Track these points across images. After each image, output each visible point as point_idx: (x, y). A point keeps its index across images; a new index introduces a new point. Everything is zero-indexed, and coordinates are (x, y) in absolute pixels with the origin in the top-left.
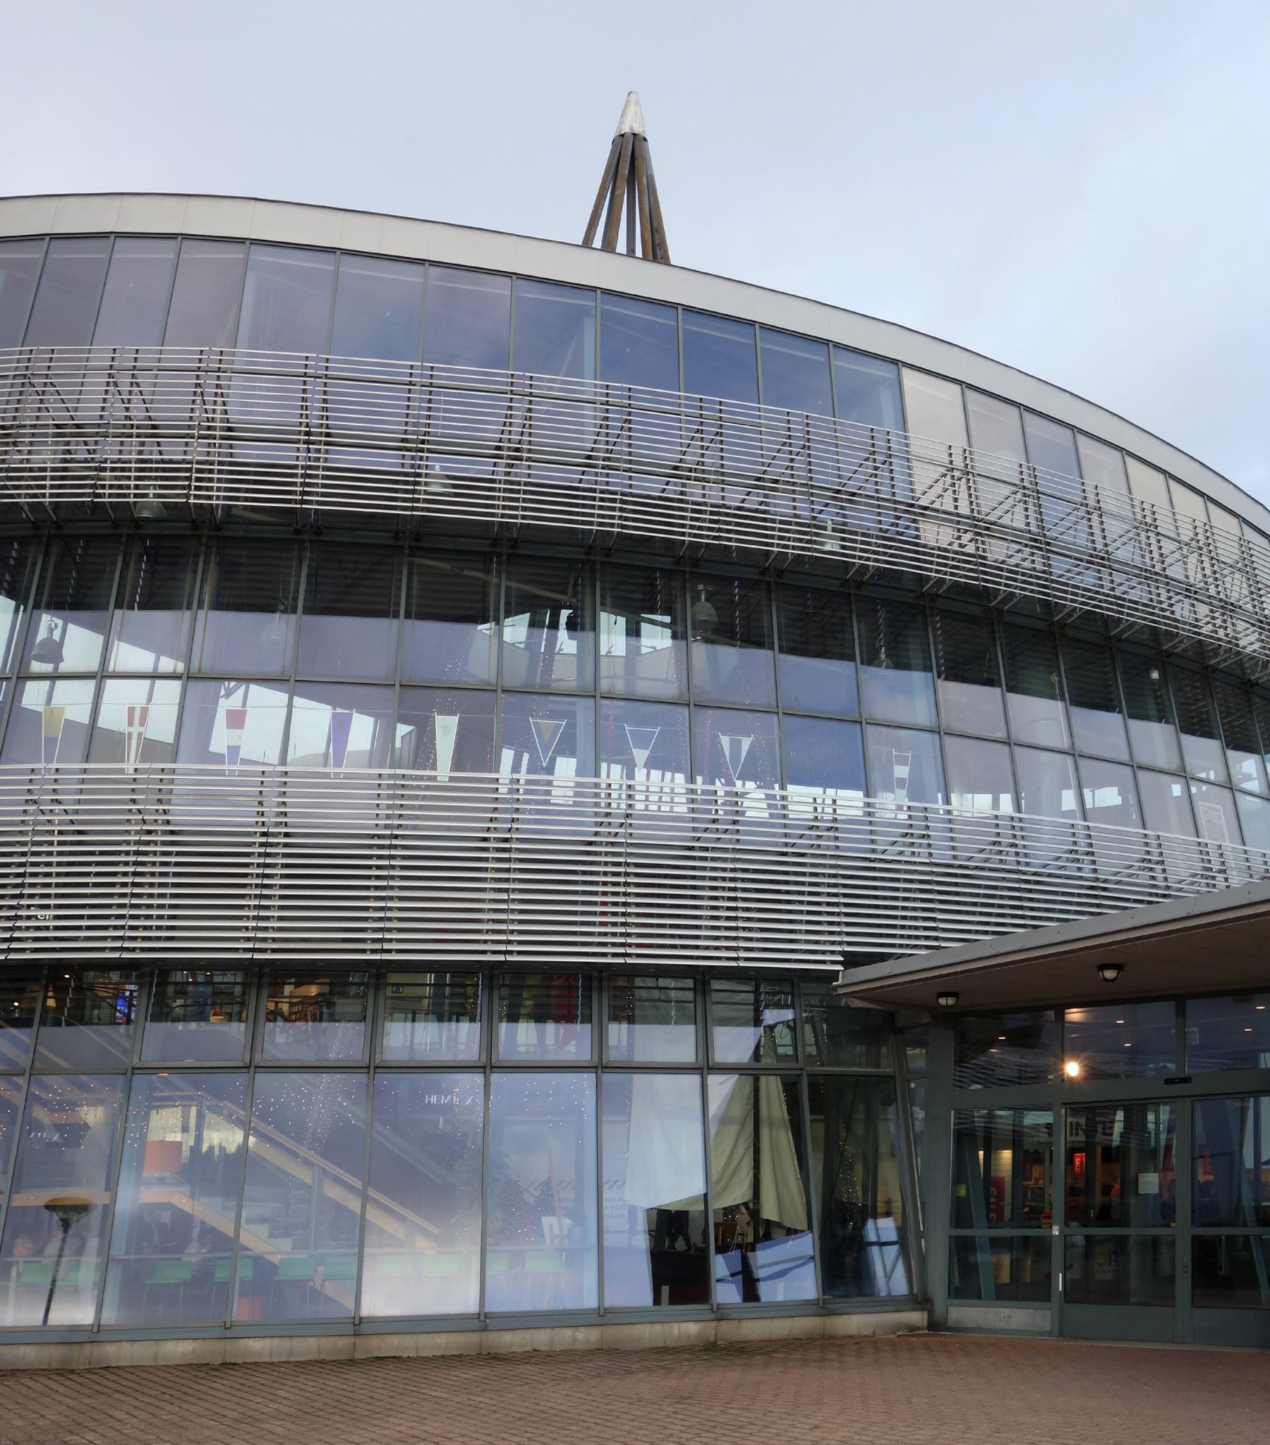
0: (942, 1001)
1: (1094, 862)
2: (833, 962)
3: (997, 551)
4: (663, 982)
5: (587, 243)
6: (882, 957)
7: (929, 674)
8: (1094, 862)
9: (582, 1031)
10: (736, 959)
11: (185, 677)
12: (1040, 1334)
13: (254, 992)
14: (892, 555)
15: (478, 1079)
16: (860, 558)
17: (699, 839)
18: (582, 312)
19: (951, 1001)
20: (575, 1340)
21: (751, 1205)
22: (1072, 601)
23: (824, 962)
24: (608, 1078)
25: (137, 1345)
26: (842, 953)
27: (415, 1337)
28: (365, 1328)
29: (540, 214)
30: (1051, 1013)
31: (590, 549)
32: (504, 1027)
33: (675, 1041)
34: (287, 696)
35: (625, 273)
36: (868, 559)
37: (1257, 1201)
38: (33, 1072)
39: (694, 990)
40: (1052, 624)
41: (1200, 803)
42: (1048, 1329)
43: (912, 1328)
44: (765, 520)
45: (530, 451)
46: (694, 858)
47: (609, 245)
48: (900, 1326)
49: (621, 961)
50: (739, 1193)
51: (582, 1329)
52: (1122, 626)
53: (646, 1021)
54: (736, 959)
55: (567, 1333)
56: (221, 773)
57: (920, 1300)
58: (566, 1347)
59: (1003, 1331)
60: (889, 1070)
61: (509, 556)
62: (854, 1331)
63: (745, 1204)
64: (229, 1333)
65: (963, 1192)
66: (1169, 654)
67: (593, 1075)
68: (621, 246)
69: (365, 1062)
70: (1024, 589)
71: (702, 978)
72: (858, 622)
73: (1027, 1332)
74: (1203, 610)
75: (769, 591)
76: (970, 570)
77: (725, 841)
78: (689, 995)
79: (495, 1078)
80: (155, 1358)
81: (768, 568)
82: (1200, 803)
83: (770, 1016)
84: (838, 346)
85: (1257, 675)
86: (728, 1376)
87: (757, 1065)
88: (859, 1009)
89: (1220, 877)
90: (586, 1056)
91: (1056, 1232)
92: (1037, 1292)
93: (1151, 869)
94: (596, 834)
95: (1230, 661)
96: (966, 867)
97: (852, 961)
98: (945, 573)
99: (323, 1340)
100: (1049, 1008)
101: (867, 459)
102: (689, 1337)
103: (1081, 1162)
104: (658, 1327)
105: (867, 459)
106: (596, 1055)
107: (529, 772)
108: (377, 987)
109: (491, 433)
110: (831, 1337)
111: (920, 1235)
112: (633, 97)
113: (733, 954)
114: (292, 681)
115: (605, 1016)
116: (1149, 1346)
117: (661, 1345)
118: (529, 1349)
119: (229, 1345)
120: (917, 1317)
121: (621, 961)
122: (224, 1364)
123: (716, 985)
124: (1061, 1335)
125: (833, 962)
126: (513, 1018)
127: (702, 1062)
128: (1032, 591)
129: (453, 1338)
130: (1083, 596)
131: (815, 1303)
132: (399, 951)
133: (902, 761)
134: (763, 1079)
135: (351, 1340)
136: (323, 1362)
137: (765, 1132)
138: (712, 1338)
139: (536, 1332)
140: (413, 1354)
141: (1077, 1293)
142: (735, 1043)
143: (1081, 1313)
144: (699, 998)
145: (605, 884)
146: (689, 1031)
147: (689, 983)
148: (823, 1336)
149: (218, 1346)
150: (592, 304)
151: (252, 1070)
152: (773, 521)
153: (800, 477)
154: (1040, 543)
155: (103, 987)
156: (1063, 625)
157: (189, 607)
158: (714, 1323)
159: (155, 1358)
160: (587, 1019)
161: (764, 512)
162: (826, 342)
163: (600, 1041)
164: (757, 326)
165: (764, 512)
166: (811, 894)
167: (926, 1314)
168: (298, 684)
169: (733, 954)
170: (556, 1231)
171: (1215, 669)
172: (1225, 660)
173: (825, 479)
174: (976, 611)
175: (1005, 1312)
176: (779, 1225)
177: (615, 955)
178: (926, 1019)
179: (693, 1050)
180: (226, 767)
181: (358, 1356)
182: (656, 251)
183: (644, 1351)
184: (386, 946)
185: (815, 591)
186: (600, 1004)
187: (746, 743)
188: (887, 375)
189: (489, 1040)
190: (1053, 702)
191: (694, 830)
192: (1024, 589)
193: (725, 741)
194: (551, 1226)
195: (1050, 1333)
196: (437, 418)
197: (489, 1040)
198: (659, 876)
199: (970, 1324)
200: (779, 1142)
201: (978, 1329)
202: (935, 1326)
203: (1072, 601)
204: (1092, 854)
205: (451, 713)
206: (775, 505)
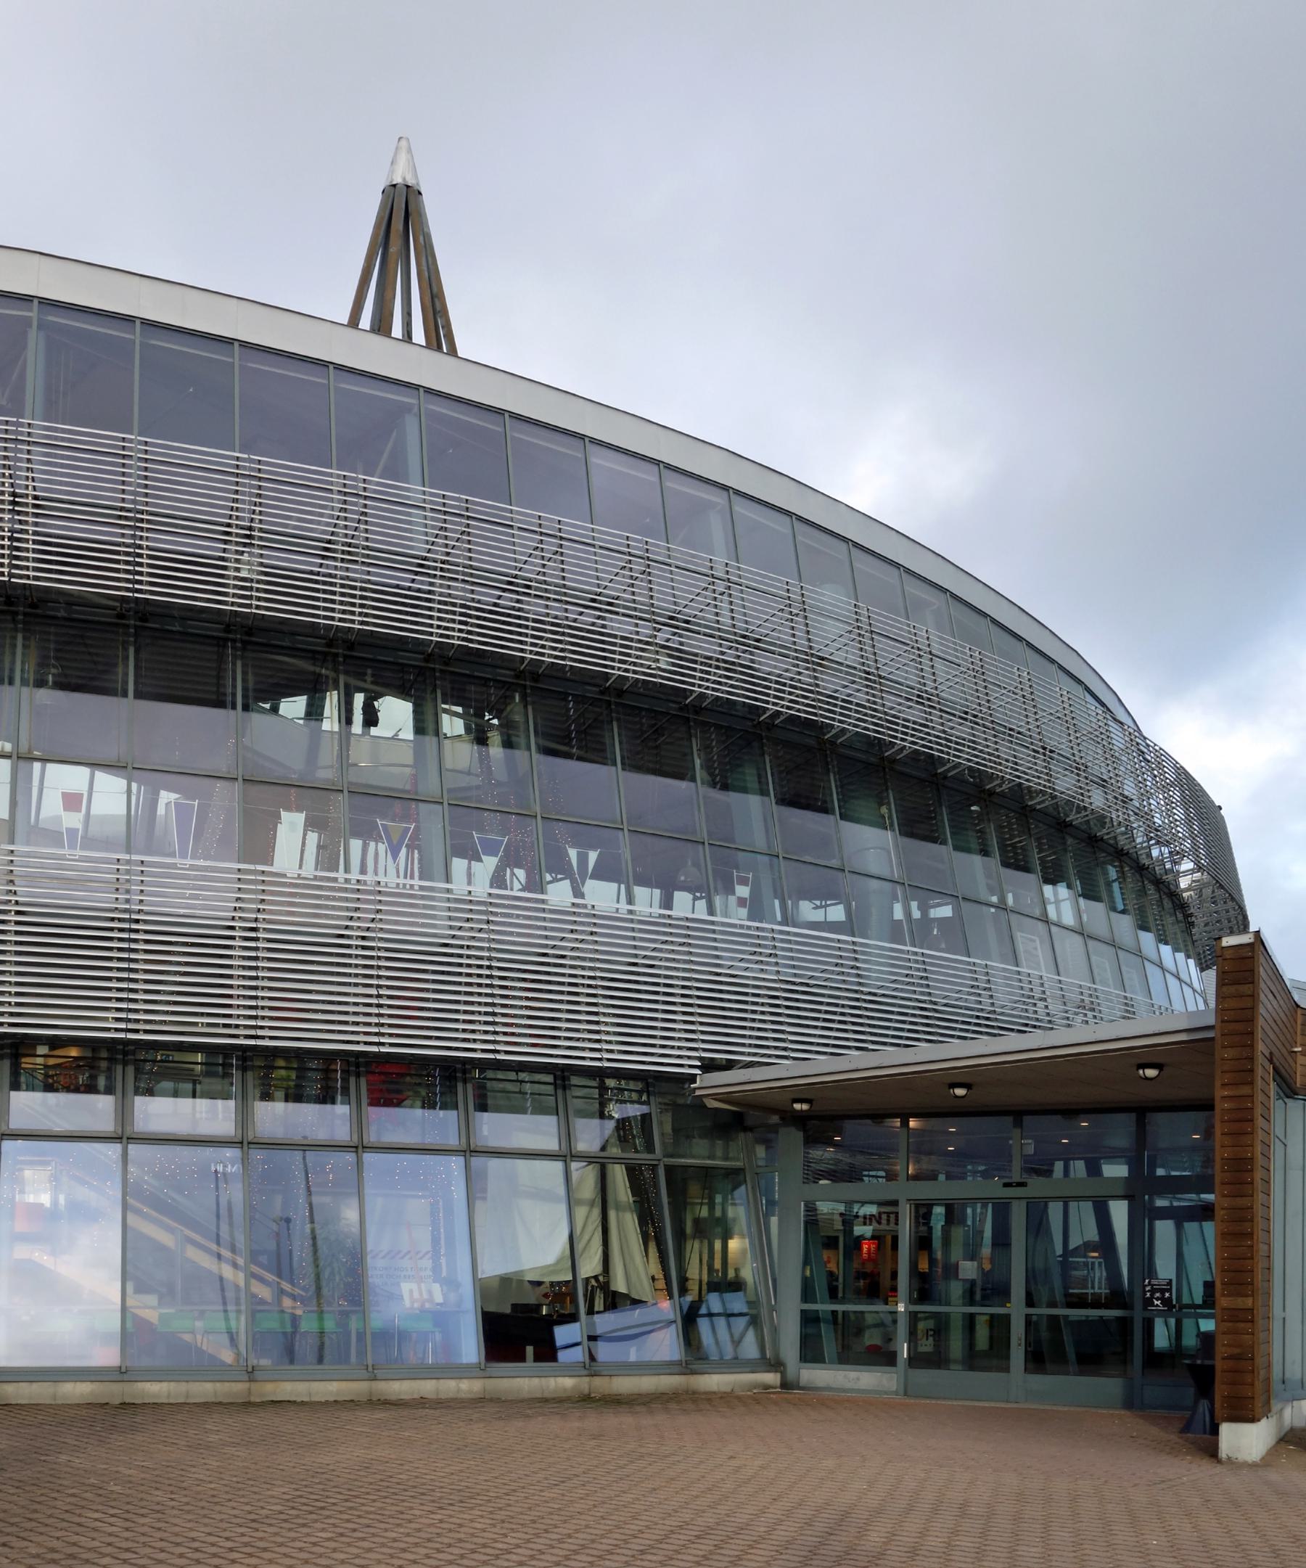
0: (797, 1106)
1: (991, 997)
2: (691, 1066)
3: (830, 683)
4: (523, 1076)
5: (354, 322)
6: (729, 1065)
7: (766, 799)
8: (991, 997)
9: (449, 1118)
10: (600, 1059)
11: (15, 757)
12: (886, 1393)
13: (119, 1068)
14: (732, 686)
15: (350, 1157)
16: (700, 686)
17: (454, 937)
18: (406, 409)
19: (805, 1107)
20: (459, 1390)
21: (601, 1278)
22: (903, 740)
23: (583, 1058)
24: (476, 1161)
25: (35, 1385)
26: (700, 1059)
27: (307, 1384)
28: (257, 1374)
29: (303, 286)
30: (897, 1122)
31: (429, 658)
32: (139, 1101)
33: (538, 1131)
34: (125, 782)
35: (402, 359)
36: (626, 670)
37: (1066, 1288)
38: (359, 1147)
39: (555, 1084)
40: (883, 758)
41: (1019, 934)
42: (894, 1389)
43: (767, 1387)
44: (519, 618)
45: (261, 530)
46: (548, 964)
47: (381, 326)
48: (756, 1385)
49: (375, 1049)
50: (590, 1266)
51: (465, 1381)
52: (949, 765)
53: (498, 1109)
54: (600, 1059)
55: (452, 1384)
56: (174, 866)
57: (776, 1364)
58: (451, 1395)
59: (859, 1391)
60: (738, 1164)
61: (345, 657)
62: (715, 1388)
63: (596, 1278)
64: (125, 1377)
65: (808, 1273)
66: (991, 793)
67: (462, 1159)
68: (397, 331)
69: (239, 1139)
70: (717, 690)
71: (562, 1076)
72: (619, 728)
73: (876, 1392)
74: (1022, 753)
75: (524, 698)
76: (807, 705)
77: (462, 938)
78: (550, 1089)
79: (368, 1157)
80: (54, 1397)
81: (523, 672)
82: (1019, 934)
83: (616, 1111)
84: (594, 441)
85: (1105, 831)
86: (593, 1421)
87: (603, 1154)
88: (716, 1109)
89: (1041, 1004)
90: (552, 1144)
91: (901, 1308)
92: (888, 1358)
93: (979, 995)
94: (347, 927)
95: (1047, 803)
96: (875, 994)
97: (709, 1066)
98: (707, 688)
99: (218, 1384)
100: (895, 1116)
101: (706, 589)
102: (565, 1390)
103: (869, 1249)
104: (536, 1381)
105: (706, 589)
106: (464, 1140)
107: (420, 879)
108: (564, 1088)
109: (320, 529)
110: (694, 1393)
111: (772, 1309)
112: (403, 143)
113: (597, 1055)
114: (130, 767)
115: (365, 1101)
116: (986, 1404)
117: (539, 1396)
118: (416, 1396)
119: (127, 1388)
120: (772, 1378)
121: (252, 1042)
122: (124, 1405)
123: (575, 1080)
124: (905, 1394)
125: (691, 1066)
126: (266, 1096)
127: (565, 1150)
128: (799, 710)
129: (344, 1385)
130: (913, 736)
131: (679, 1363)
132: (391, 1045)
133: (744, 882)
134: (610, 1167)
135: (247, 1385)
136: (220, 1403)
137: (612, 1215)
138: (586, 1391)
139: (423, 1382)
140: (306, 1399)
141: (916, 1360)
142: (590, 1135)
143: (924, 1376)
144: (560, 1092)
145: (379, 977)
146: (550, 1122)
147: (549, 1078)
148: (687, 1392)
149: (116, 1388)
150: (414, 401)
151: (125, 1140)
152: (527, 619)
153: (552, 576)
154: (873, 679)
155: (499, 1083)
156: (893, 761)
157: (11, 683)
158: (587, 1379)
159: (54, 1397)
160: (109, 1091)
161: (519, 610)
162: (582, 437)
163: (244, 1117)
164: (507, 415)
165: (519, 610)
166: (825, 1020)
167: (779, 1375)
168: (136, 772)
169: (597, 1055)
170: (416, 1295)
171: (1033, 809)
172: (1043, 802)
173: (663, 604)
174: (812, 742)
175: (853, 1375)
176: (626, 1296)
177: (247, 1037)
178: (775, 1119)
179: (556, 1141)
180: (177, 861)
181: (253, 1399)
182: (439, 335)
183: (522, 1401)
184: (260, 1033)
185: (718, 727)
186: (465, 1093)
187: (593, 856)
188: (718, 500)
189: (124, 1113)
190: (884, 832)
191: (451, 927)
192: (717, 690)
193: (573, 853)
194: (411, 1291)
195: (896, 1393)
196: (328, 524)
197: (124, 1113)
198: (193, 945)
199: (821, 1384)
200: (627, 1224)
201: (829, 1389)
202: (785, 1385)
203: (903, 740)
204: (990, 989)
205: (299, 810)
206: (760, 663)
